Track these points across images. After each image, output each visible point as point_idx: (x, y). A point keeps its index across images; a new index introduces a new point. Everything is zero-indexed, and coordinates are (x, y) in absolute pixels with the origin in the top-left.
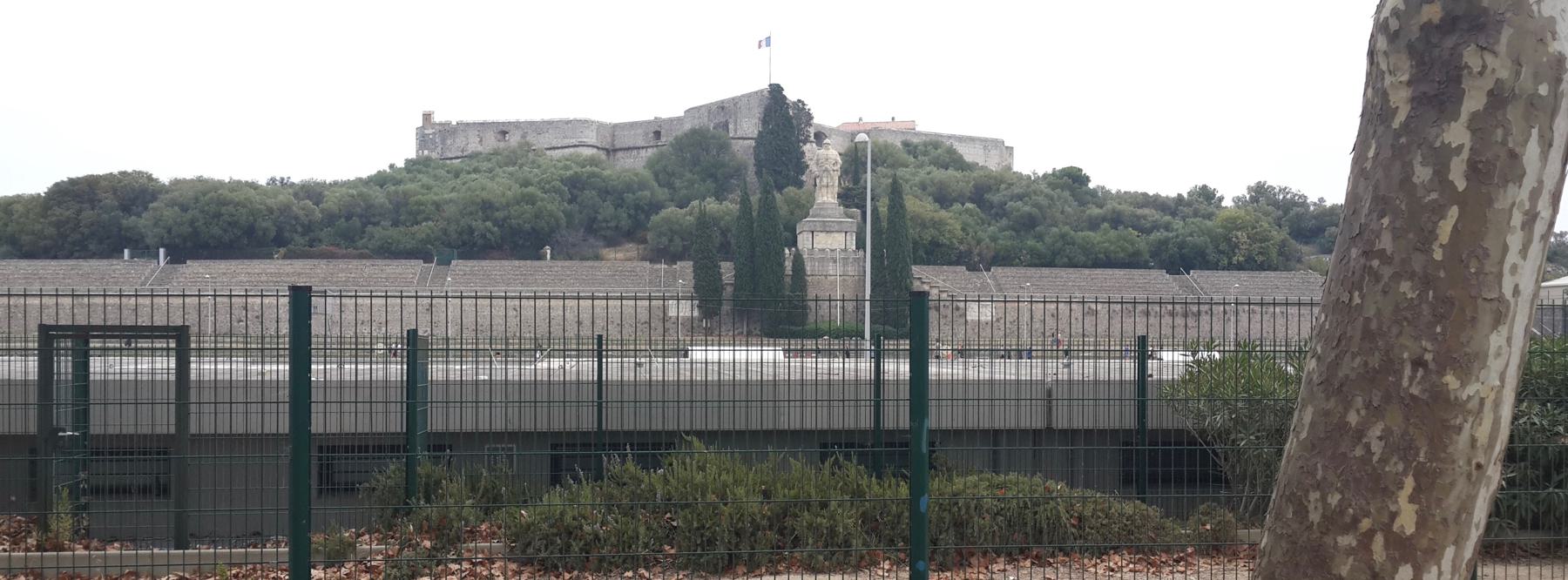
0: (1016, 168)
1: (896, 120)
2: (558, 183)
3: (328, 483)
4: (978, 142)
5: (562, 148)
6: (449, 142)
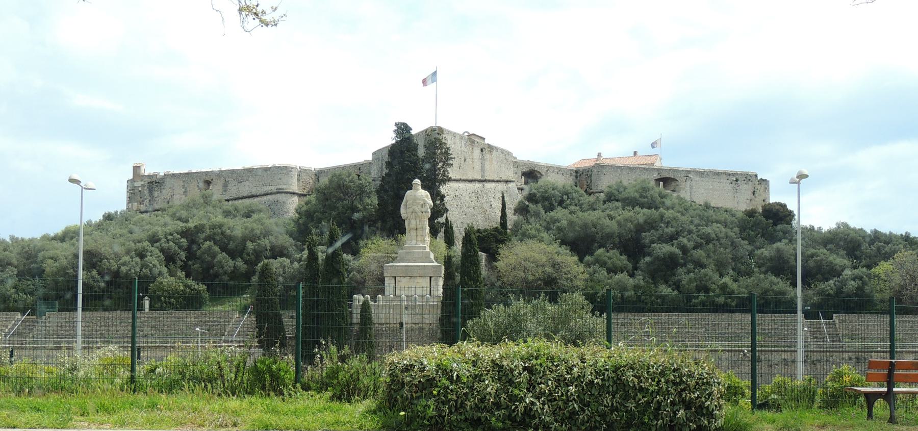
0: (771, 202)
1: (638, 154)
4: (725, 176)
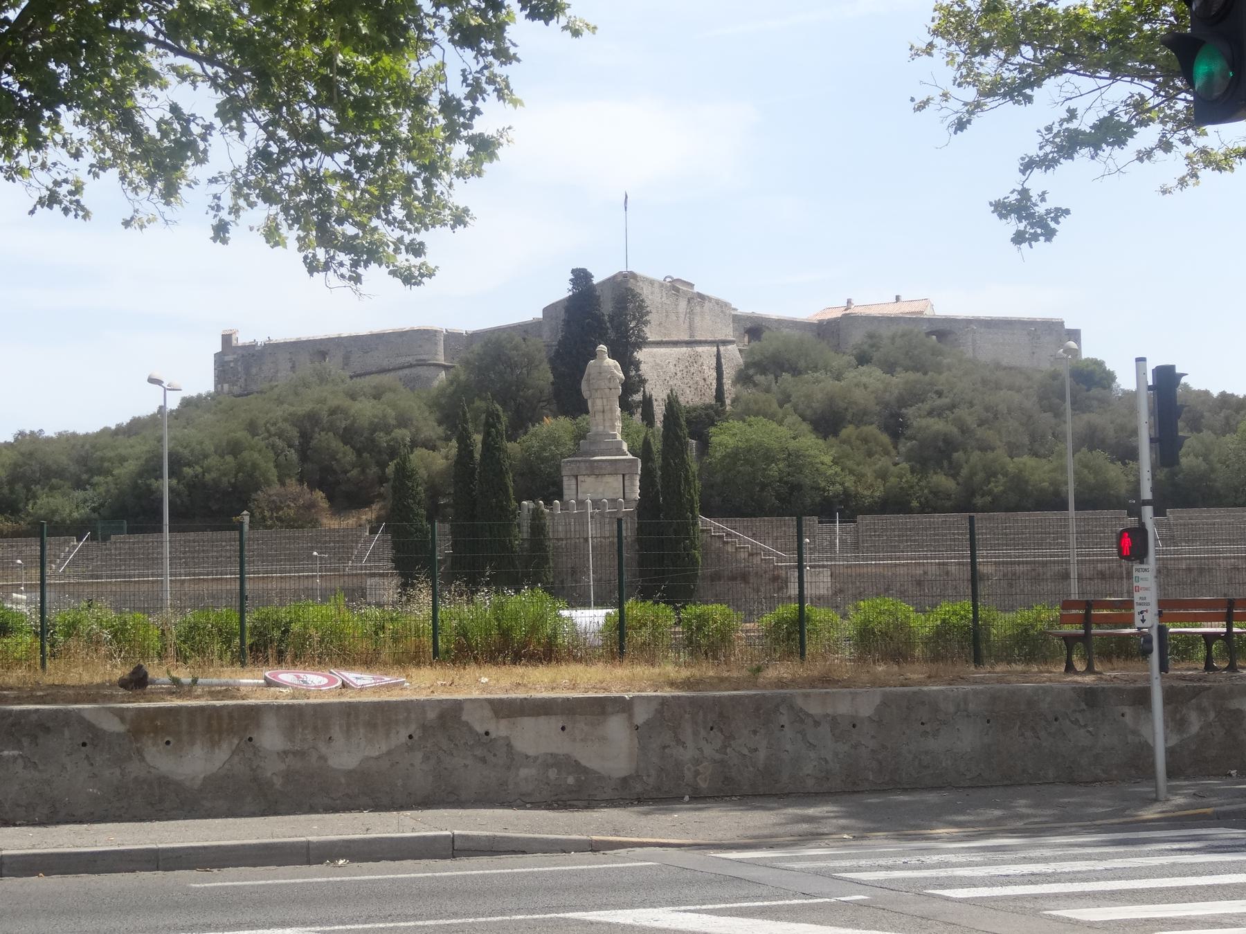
1: (903, 299)
2: (287, 426)
3: (1082, 555)
5: (394, 369)
6: (254, 371)
